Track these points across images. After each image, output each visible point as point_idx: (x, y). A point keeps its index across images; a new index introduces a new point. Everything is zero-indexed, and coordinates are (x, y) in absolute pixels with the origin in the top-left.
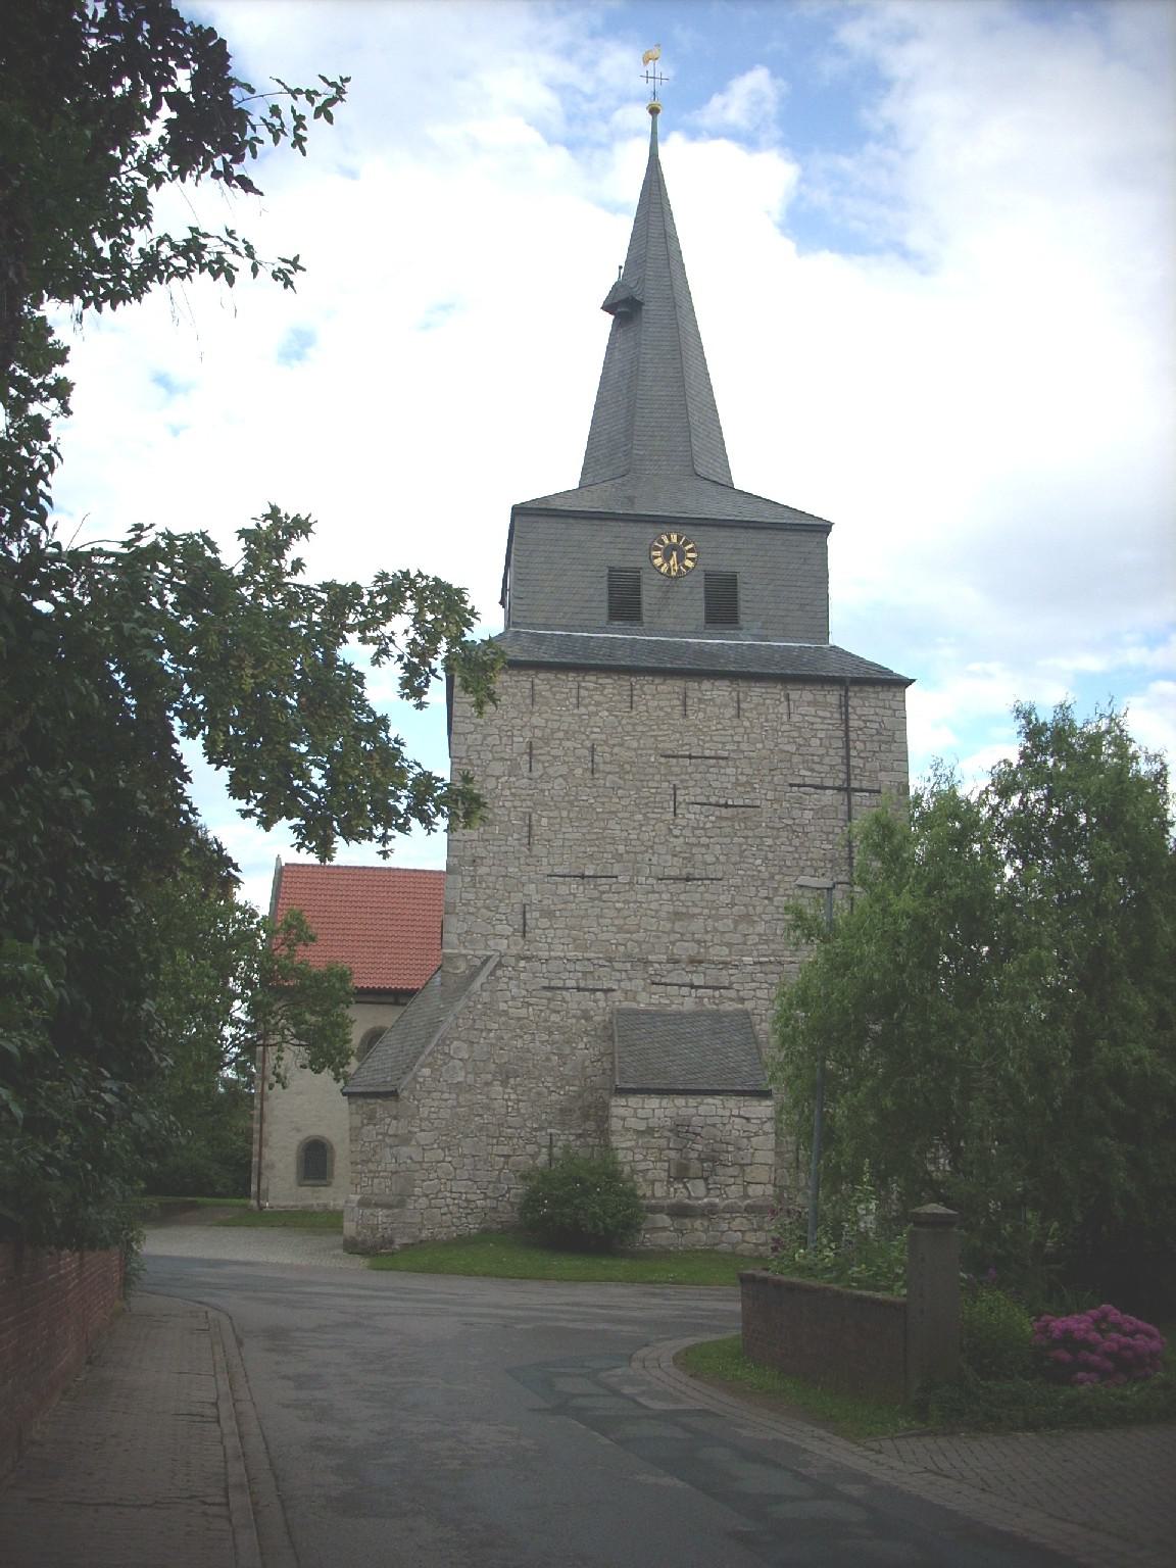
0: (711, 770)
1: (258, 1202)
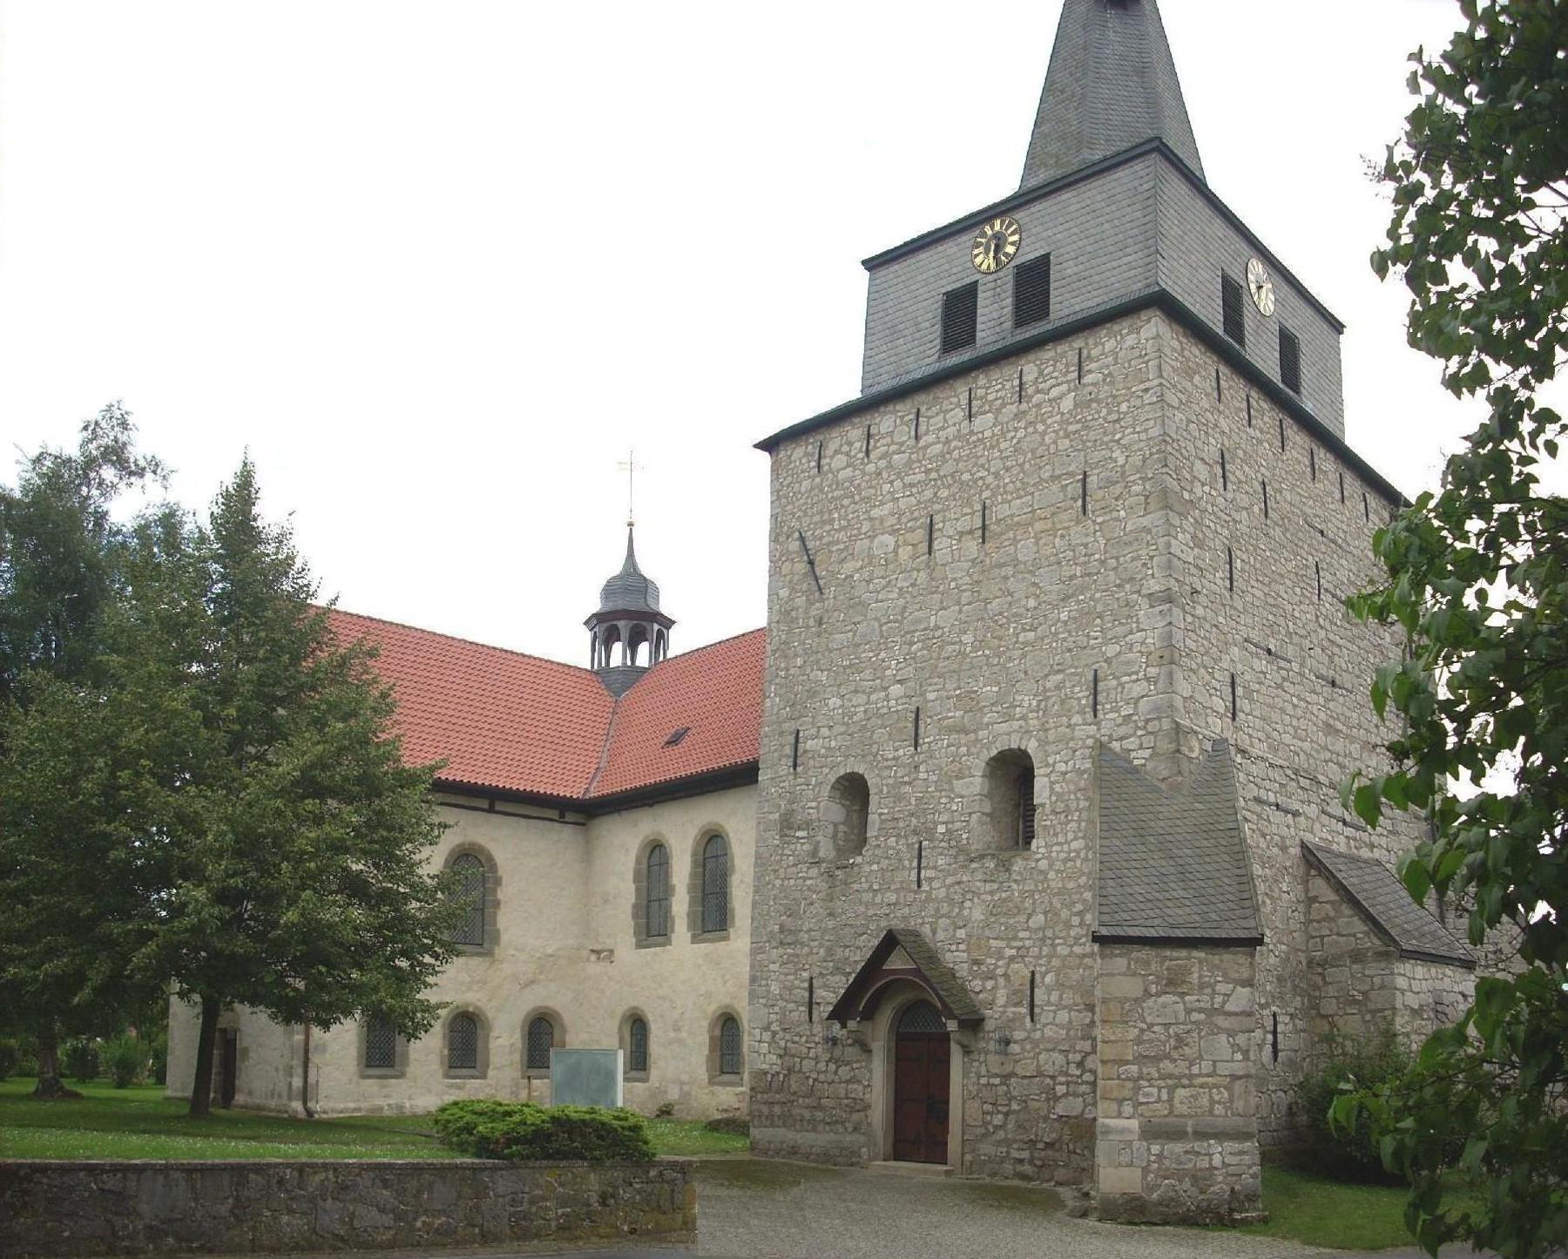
0: (1251, 491)
1: (305, 1102)
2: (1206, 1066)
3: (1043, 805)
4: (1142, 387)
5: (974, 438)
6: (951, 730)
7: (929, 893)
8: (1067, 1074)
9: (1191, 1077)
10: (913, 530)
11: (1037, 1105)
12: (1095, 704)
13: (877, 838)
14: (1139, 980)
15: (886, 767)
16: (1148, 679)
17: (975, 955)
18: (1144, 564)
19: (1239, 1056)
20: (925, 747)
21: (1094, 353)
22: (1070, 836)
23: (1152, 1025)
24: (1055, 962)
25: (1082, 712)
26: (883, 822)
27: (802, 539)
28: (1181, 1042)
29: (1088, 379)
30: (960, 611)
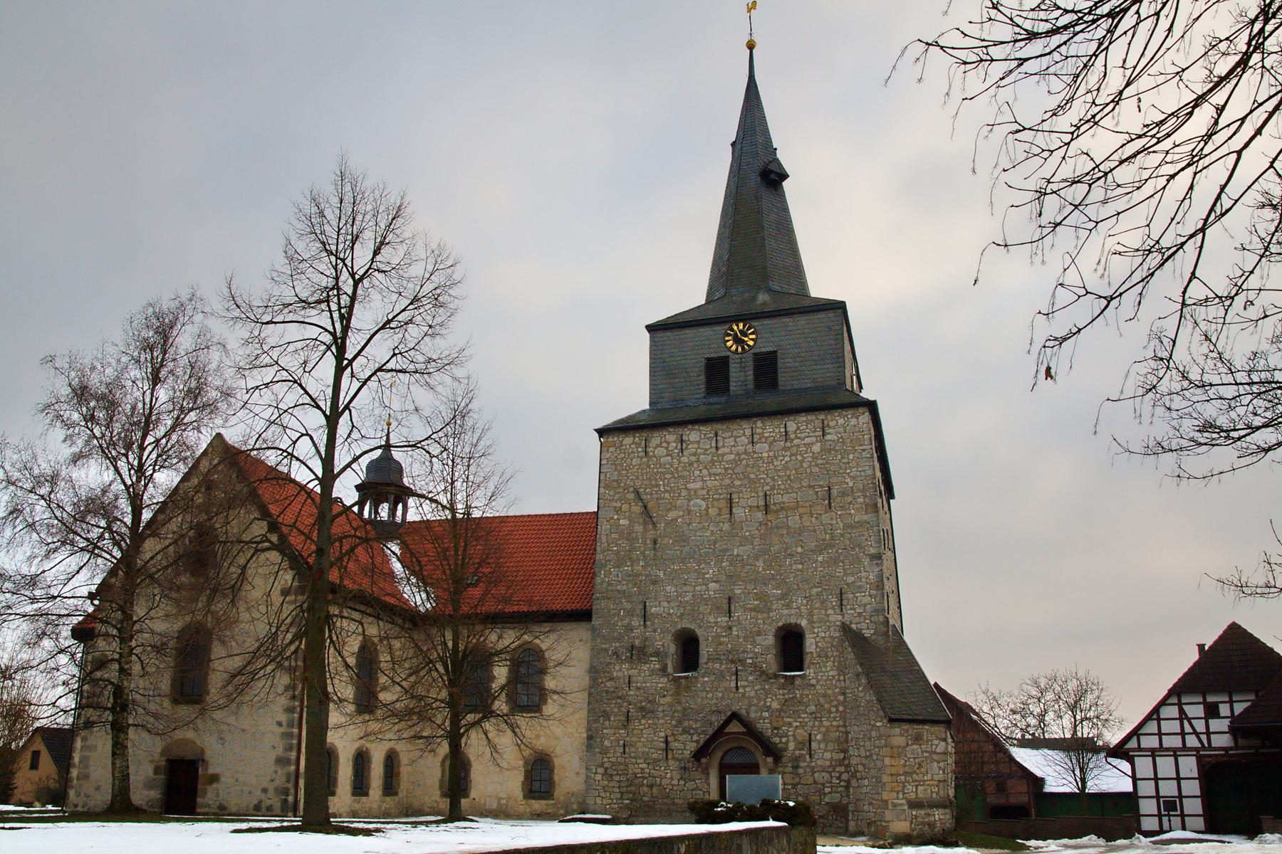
2: (929, 777)
3: (812, 653)
4: (861, 448)
5: (755, 456)
6: (751, 610)
7: (744, 695)
8: (831, 782)
9: (924, 781)
10: (718, 500)
11: (813, 798)
12: (841, 604)
13: (706, 663)
14: (904, 738)
15: (710, 627)
16: (871, 596)
17: (775, 724)
18: (866, 539)
19: (941, 772)
20: (735, 618)
21: (831, 424)
22: (829, 669)
23: (909, 758)
24: (822, 729)
25: (833, 608)
26: (709, 655)
27: (637, 493)
28: (920, 766)
29: (828, 437)
30: (754, 549)
